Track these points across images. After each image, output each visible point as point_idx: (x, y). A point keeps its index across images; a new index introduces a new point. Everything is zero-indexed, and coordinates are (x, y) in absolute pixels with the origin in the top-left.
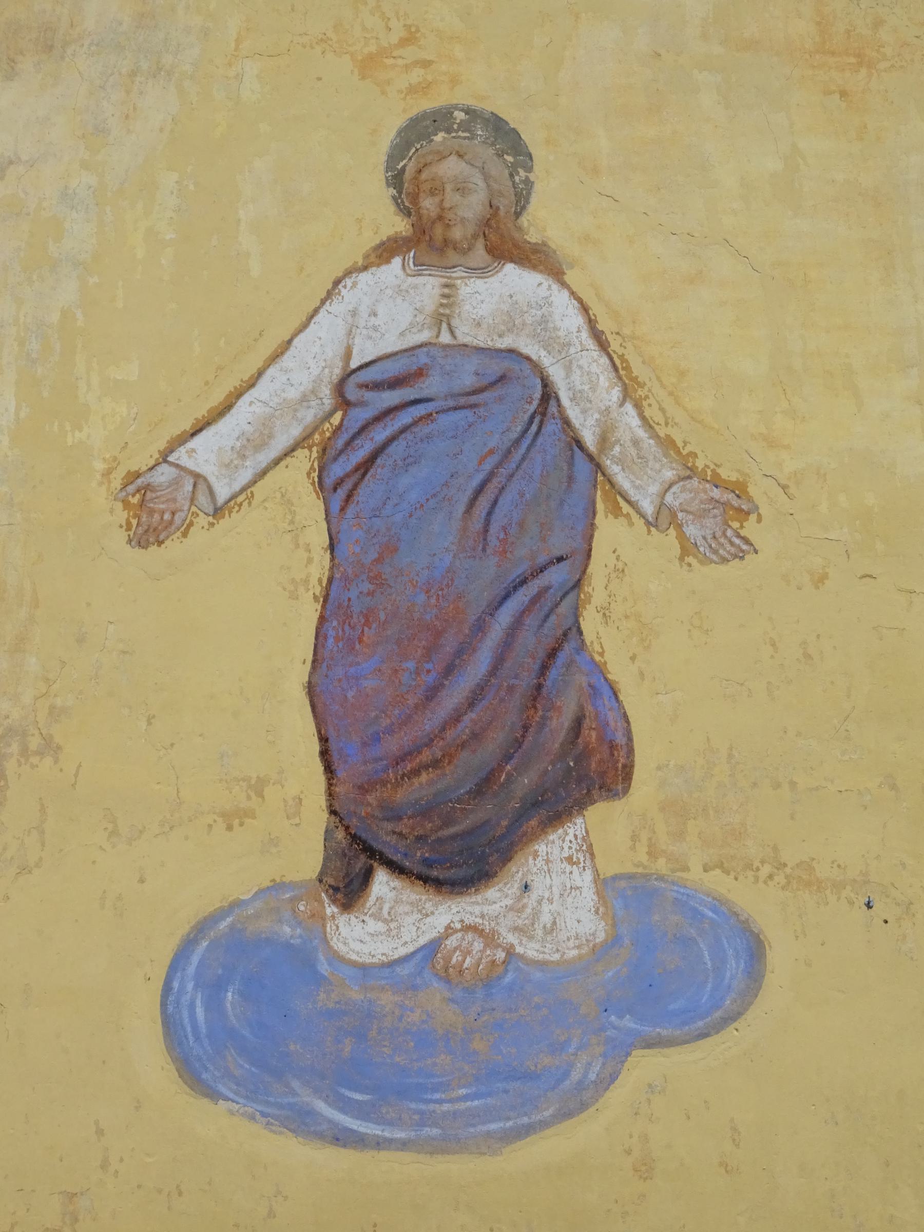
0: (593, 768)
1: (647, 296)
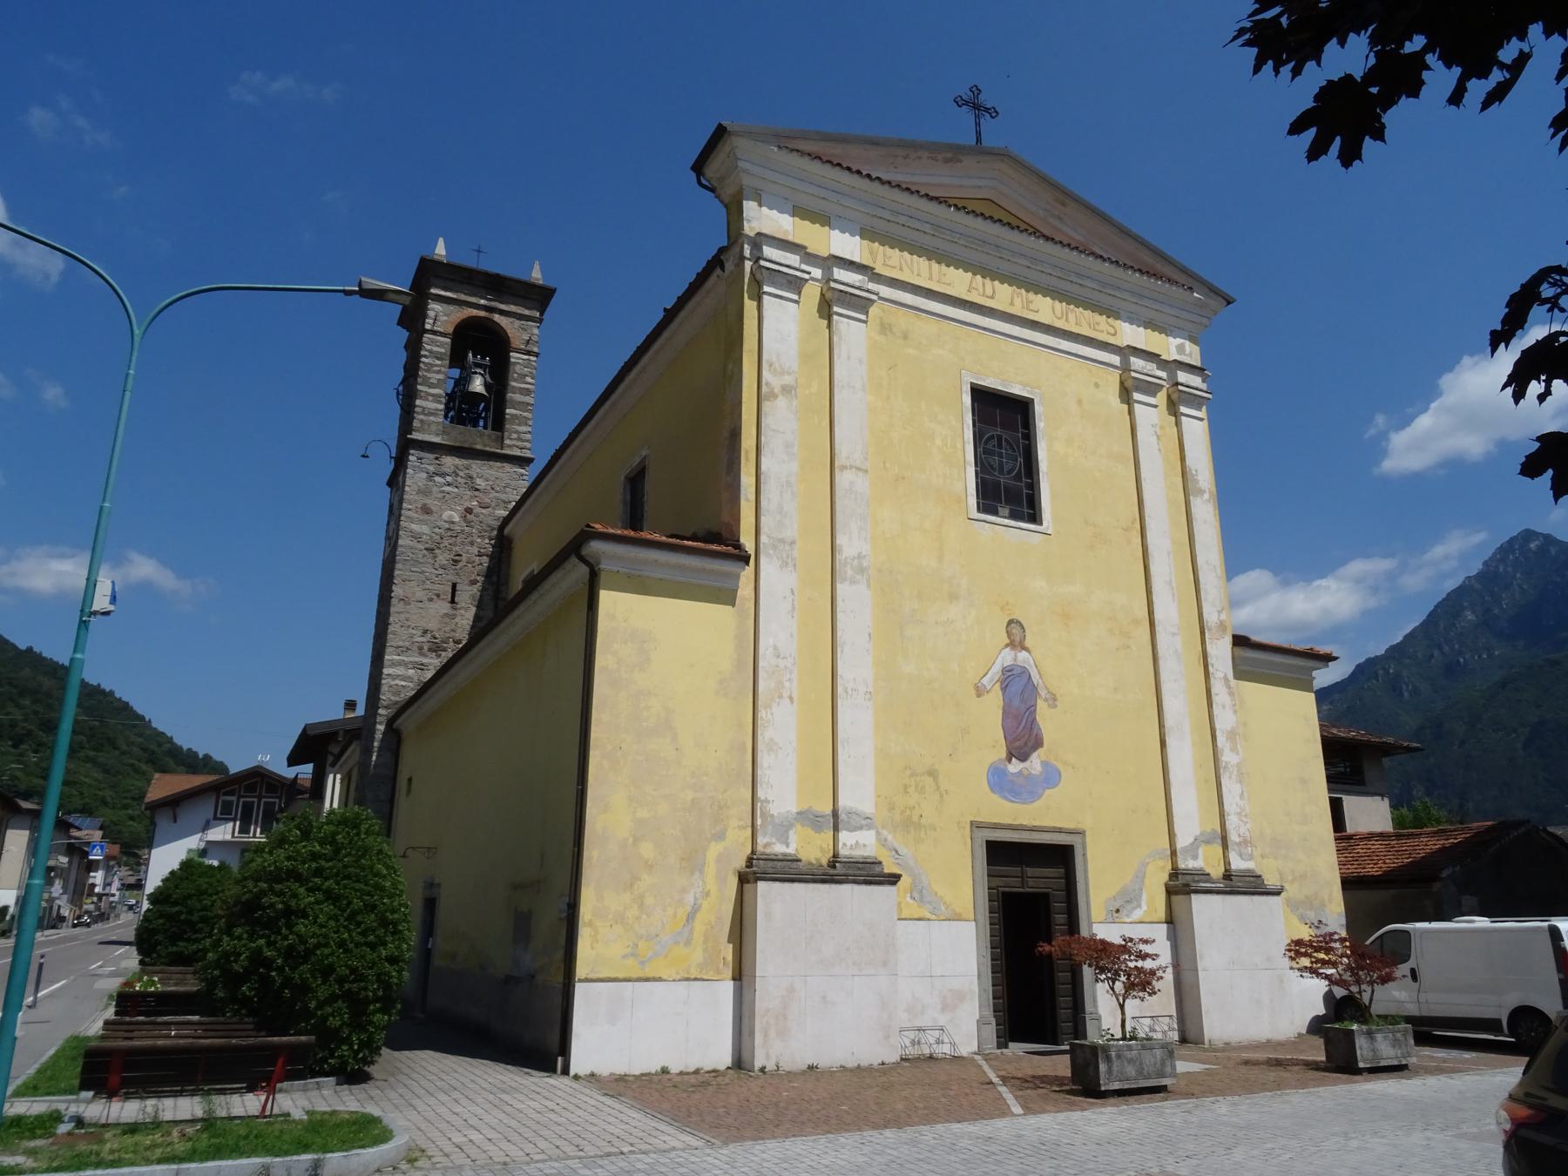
0: (1038, 744)
1: (1046, 660)
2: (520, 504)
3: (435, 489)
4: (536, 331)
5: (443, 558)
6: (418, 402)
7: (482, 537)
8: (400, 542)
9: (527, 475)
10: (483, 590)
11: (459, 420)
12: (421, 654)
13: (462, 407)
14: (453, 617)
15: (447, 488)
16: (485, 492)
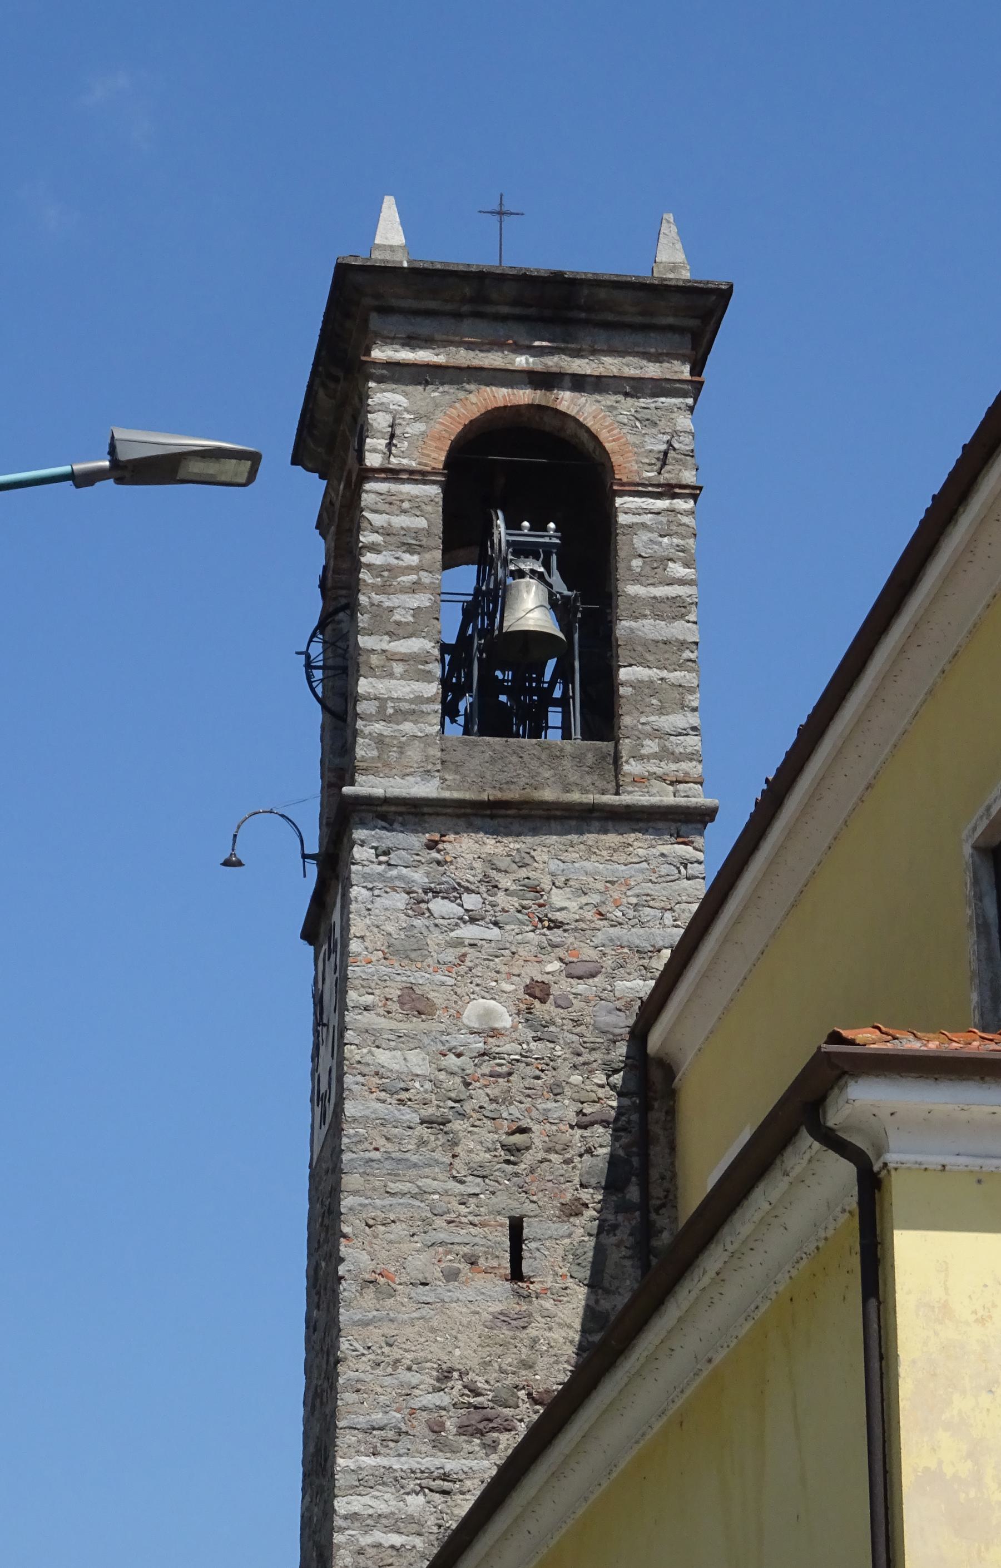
2: (685, 952)
3: (435, 938)
4: (684, 422)
5: (477, 1143)
6: (364, 686)
7: (584, 1067)
8: (350, 1108)
9: (708, 852)
10: (604, 1228)
11: (491, 721)
12: (440, 1444)
13: (494, 683)
14: (521, 1322)
15: (469, 932)
16: (580, 929)
